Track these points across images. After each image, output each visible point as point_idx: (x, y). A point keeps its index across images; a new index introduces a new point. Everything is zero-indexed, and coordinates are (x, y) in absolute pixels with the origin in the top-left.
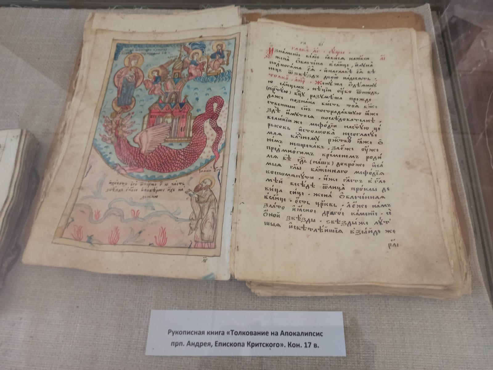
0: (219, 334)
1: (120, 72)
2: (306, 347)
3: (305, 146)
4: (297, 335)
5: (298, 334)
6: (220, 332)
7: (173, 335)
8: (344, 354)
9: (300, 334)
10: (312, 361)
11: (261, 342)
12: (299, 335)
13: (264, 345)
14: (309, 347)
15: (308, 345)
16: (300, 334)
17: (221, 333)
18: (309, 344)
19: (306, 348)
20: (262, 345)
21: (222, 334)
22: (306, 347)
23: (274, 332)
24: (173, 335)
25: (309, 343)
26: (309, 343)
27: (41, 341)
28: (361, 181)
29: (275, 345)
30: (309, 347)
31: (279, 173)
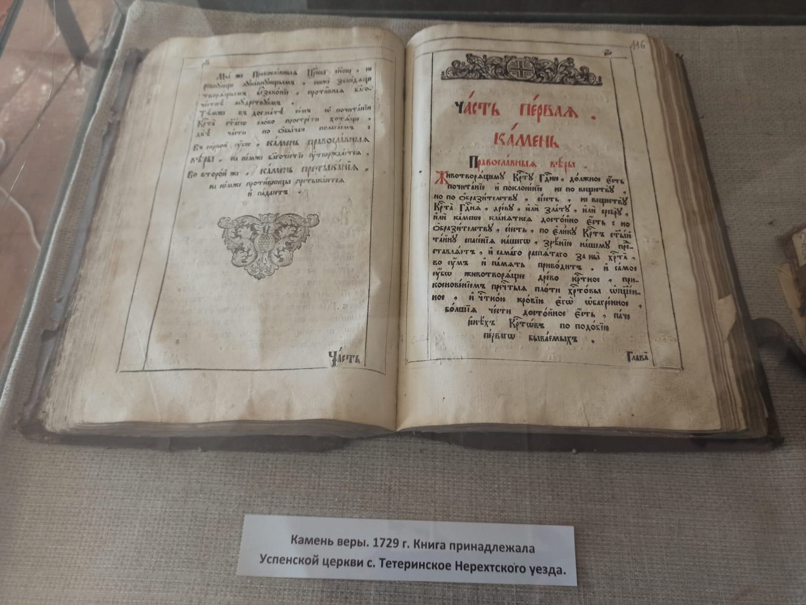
0: (437, 548)
1: (537, 141)
2: (376, 546)
3: (627, 293)
4: (517, 551)
5: (519, 550)
6: (437, 544)
7: (532, 575)
8: (576, 585)
9: (522, 550)
10: (7, 528)
11: (492, 564)
12: (520, 551)
13: (499, 569)
14: (382, 546)
15: (380, 542)
16: (522, 550)
17: (439, 546)
18: (382, 541)
19: (376, 548)
20: (494, 568)
21: (441, 548)
22: (376, 546)
23: (476, 545)
24: (532, 575)
25: (381, 539)
26: (381, 539)
27: (65, 556)
28: (593, 315)
29: (518, 569)
30: (382, 546)
31: (565, 302)
